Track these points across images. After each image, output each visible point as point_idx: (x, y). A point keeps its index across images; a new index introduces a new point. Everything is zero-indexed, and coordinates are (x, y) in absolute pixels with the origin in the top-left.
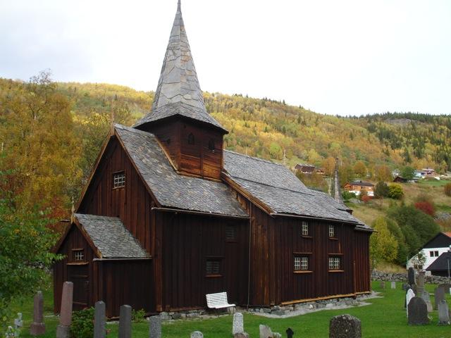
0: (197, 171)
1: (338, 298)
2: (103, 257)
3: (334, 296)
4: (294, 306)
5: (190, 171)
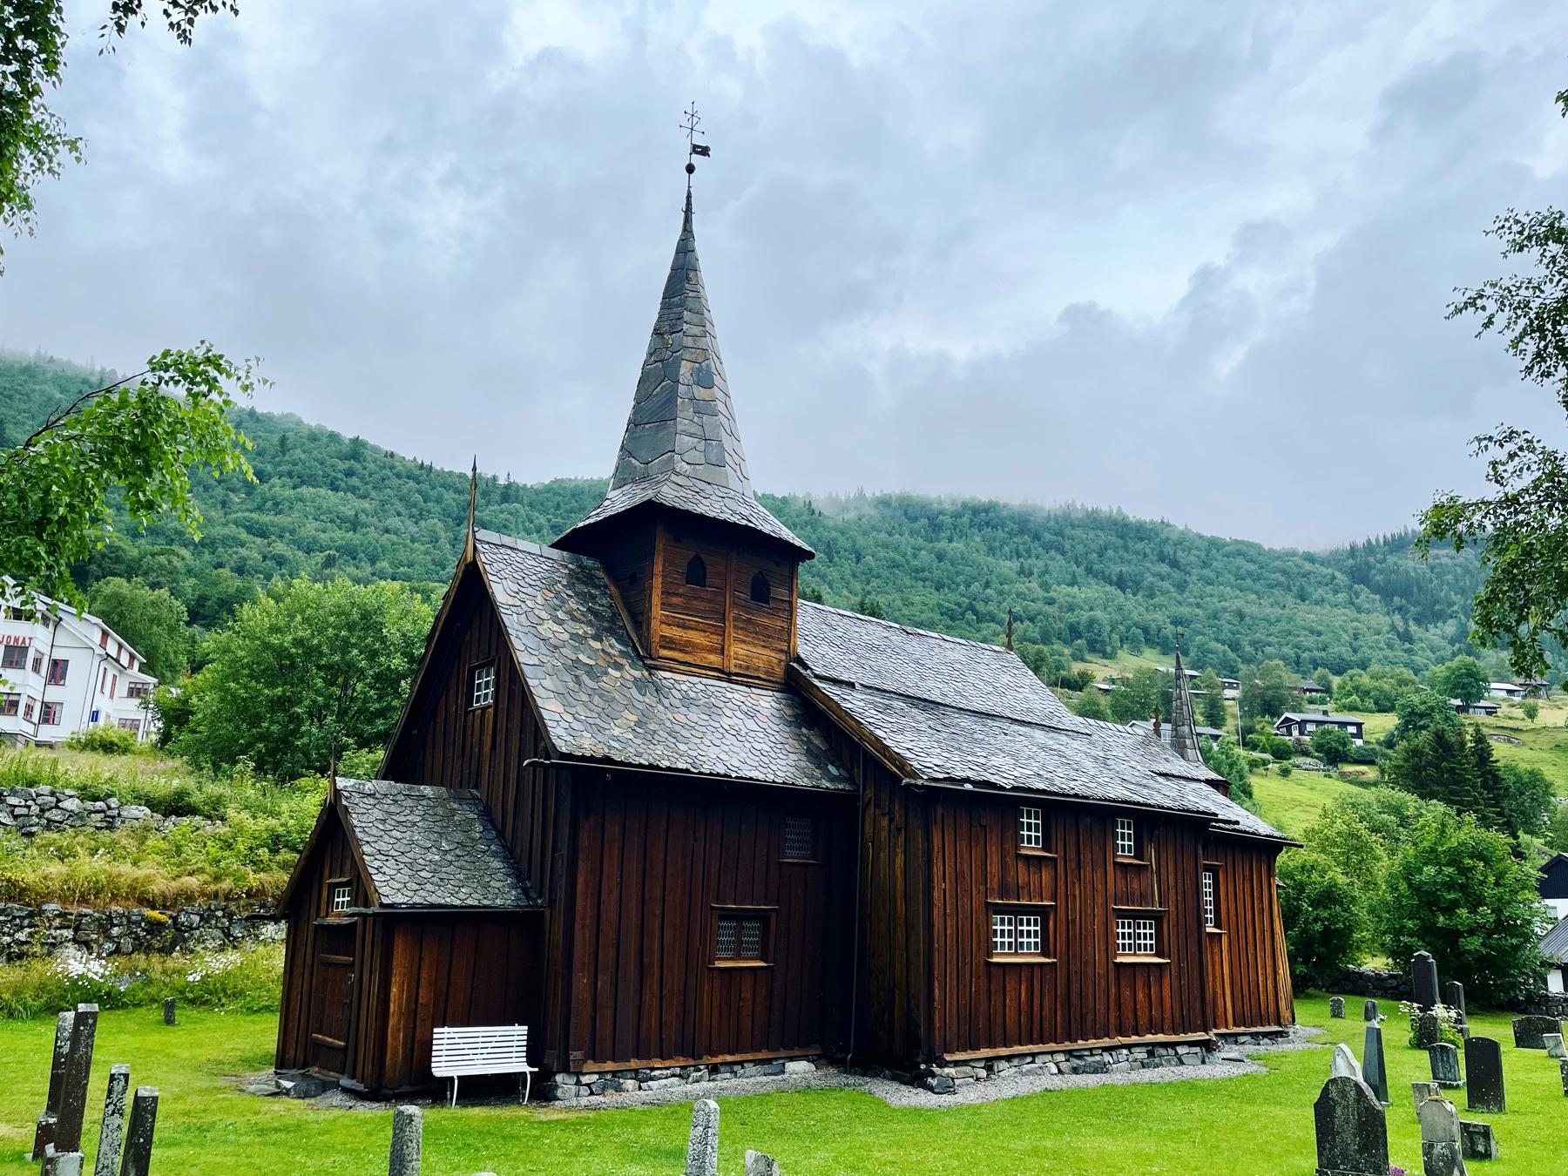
0: (714, 659)
1: (1154, 1045)
2: (382, 905)
3: (1134, 1039)
4: (989, 1069)
5: (688, 658)
